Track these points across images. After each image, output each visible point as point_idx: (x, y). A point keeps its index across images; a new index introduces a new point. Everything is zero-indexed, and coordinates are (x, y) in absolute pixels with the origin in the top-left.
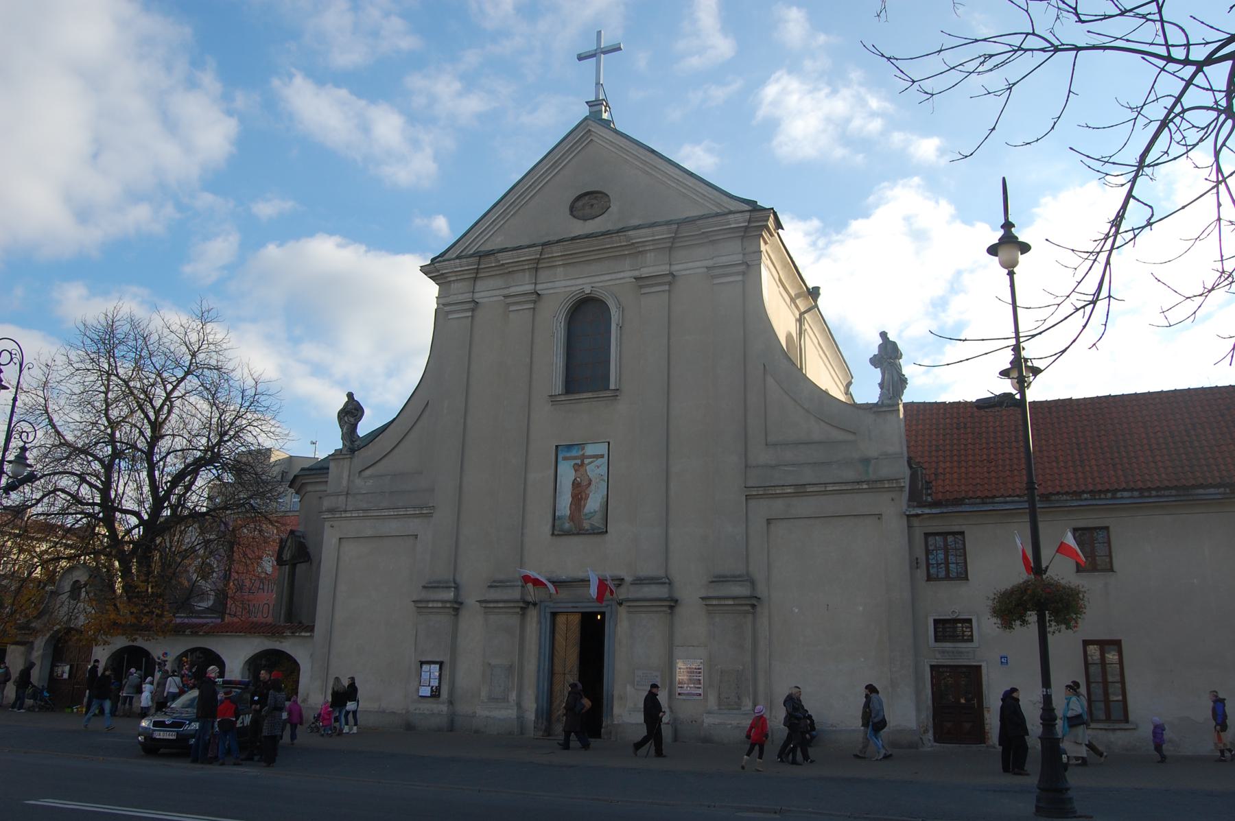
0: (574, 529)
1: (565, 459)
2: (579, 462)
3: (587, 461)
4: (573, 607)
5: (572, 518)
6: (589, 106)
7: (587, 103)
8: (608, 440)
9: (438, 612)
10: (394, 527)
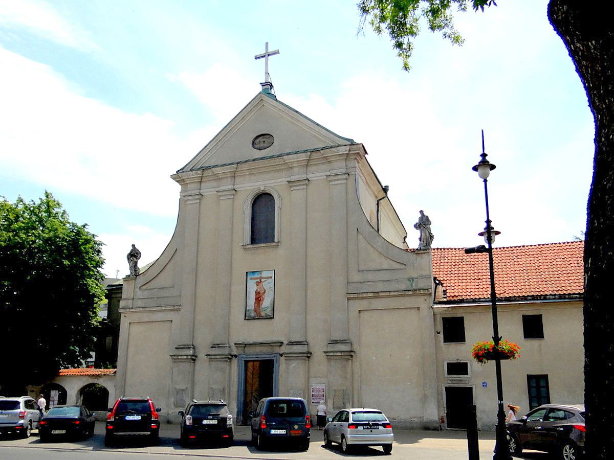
1: (251, 279)
2: (259, 280)
3: (263, 280)
4: (256, 357)
5: (255, 311)
6: (262, 86)
7: (261, 84)
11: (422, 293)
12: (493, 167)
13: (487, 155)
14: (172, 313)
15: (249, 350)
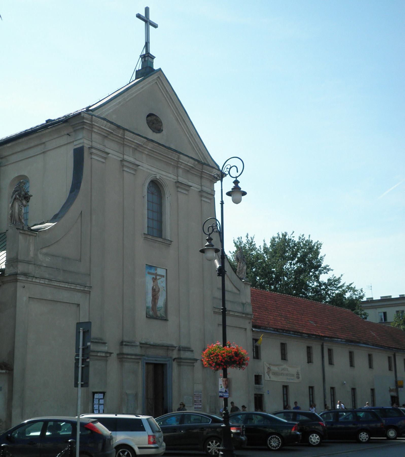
0: (154, 316)
2: (154, 276)
4: (156, 360)
8: (166, 268)
9: (97, 359)
10: (64, 296)
11: (249, 317)
12: (244, 193)
13: (239, 182)
14: (79, 294)
15: (151, 352)
